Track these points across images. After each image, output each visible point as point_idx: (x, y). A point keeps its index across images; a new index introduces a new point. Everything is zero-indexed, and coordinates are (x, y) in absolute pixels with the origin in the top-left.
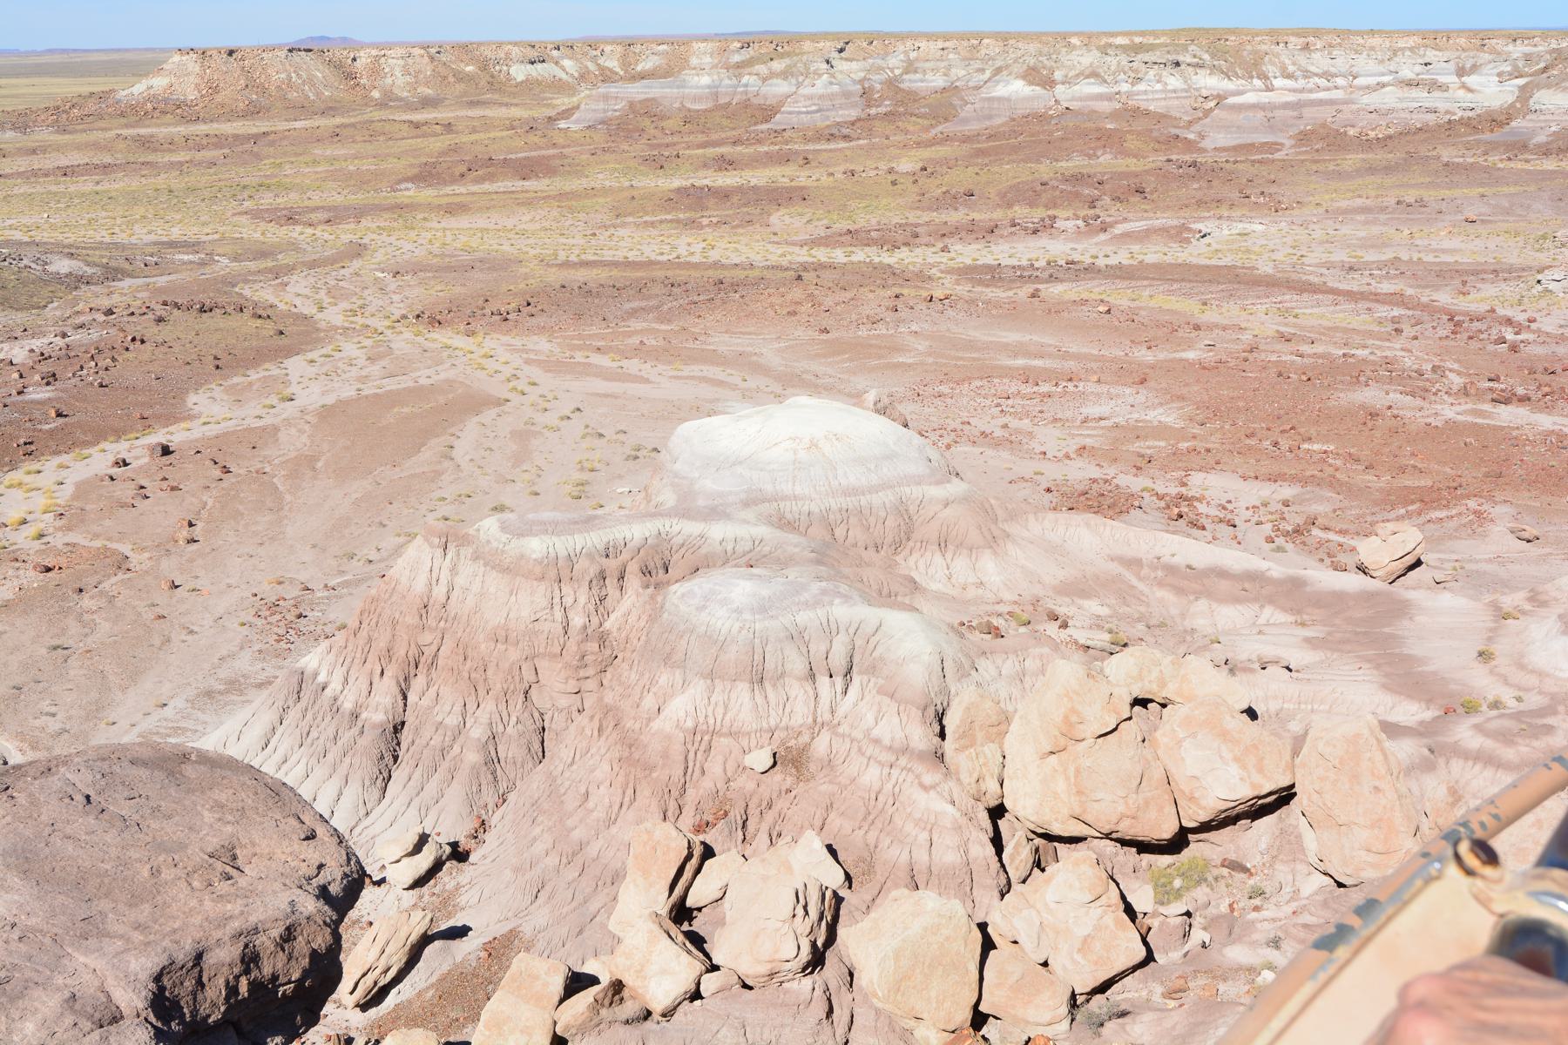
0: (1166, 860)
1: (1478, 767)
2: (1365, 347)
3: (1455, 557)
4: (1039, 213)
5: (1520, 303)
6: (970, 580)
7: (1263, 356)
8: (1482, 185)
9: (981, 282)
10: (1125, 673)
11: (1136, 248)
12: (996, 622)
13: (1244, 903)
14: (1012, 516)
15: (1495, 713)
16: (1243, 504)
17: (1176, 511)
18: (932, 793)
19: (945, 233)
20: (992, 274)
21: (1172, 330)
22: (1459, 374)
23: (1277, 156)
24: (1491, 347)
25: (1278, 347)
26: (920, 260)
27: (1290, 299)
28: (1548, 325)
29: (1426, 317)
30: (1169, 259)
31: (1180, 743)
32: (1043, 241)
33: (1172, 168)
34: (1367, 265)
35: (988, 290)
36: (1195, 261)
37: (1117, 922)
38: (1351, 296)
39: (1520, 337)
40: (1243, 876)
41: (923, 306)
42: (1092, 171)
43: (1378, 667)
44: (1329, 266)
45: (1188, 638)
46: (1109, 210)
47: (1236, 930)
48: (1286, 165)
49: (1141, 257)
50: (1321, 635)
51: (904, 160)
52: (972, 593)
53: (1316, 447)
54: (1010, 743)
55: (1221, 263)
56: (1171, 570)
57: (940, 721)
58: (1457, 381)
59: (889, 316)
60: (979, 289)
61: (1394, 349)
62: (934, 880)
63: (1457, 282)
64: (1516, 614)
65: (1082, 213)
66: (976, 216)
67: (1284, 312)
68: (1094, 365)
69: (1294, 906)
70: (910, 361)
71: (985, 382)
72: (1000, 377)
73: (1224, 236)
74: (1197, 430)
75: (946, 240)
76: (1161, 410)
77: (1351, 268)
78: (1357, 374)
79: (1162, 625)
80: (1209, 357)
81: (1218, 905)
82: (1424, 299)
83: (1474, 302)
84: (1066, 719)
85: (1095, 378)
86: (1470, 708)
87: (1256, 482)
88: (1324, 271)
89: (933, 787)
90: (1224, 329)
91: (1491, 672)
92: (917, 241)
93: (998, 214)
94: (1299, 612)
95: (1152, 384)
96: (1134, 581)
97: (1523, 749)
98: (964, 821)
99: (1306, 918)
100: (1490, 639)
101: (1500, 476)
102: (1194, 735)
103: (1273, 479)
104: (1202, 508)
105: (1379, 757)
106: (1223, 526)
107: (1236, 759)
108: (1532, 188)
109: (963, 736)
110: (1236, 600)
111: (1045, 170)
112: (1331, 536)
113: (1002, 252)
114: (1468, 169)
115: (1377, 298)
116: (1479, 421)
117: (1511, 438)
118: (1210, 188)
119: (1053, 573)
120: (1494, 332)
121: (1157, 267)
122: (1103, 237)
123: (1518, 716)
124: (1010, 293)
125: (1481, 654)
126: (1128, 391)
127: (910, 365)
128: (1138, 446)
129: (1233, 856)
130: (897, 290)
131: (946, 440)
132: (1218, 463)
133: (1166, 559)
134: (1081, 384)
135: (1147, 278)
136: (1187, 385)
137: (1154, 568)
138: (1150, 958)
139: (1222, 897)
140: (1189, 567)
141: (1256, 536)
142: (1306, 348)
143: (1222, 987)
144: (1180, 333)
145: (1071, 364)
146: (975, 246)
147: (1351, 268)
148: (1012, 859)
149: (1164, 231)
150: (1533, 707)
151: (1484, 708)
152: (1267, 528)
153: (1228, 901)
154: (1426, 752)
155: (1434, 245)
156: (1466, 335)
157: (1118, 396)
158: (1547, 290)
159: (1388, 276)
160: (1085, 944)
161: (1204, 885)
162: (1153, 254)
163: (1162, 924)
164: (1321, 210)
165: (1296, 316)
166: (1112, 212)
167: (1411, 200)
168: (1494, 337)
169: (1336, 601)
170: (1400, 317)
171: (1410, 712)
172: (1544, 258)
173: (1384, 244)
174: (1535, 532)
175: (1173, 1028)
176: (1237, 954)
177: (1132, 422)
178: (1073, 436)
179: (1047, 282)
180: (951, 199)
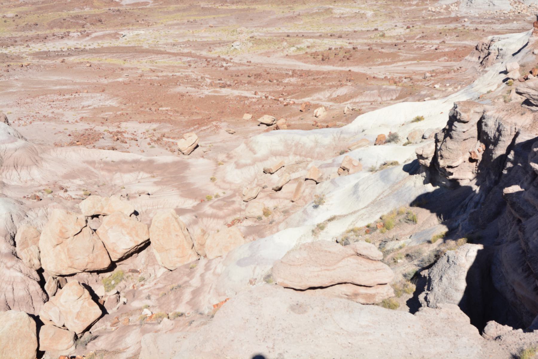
0: (108, 274)
1: (212, 219)
2: (179, 72)
3: (210, 142)
4: (64, 31)
5: (227, 53)
6: (28, 179)
7: (145, 78)
8: (214, 14)
9: (42, 58)
10: (87, 207)
11: (100, 42)
12: (37, 194)
13: (138, 284)
14: (44, 151)
15: (216, 199)
16: (140, 132)
17: (116, 137)
18: (12, 270)
19: (28, 40)
20: (47, 55)
21: (113, 71)
22: (209, 78)
23: (148, 6)
24: (219, 69)
25: (150, 74)
26: (18, 51)
27: (154, 57)
28: (236, 60)
29: (199, 60)
30: (112, 45)
31: (107, 231)
32: (65, 41)
33: (111, 12)
34: (179, 43)
35: (45, 61)
36: (121, 45)
37: (90, 304)
38: (175, 54)
39: (228, 65)
40: (137, 274)
41: (19, 69)
42: (82, 14)
43: (179, 189)
44: (167, 44)
45: (114, 188)
46: (89, 28)
47: (136, 294)
48: (151, 10)
49: (102, 45)
50: (160, 180)
51: (9, 12)
52: (29, 183)
53: (164, 109)
54: (41, 244)
55: (130, 45)
56: (106, 163)
57: (14, 239)
58: (209, 81)
59: (6, 74)
60: (42, 61)
61: (188, 72)
62: (16, 304)
63: (208, 47)
64: (223, 163)
65: (79, 30)
66: (39, 33)
67: (152, 61)
68: (86, 86)
69: (155, 281)
70: (15, 91)
71: (44, 96)
72: (50, 94)
73: (130, 36)
74: (123, 107)
75: (28, 43)
76: (110, 101)
77: (174, 45)
78: (176, 81)
79: (104, 185)
80: (127, 80)
81: (129, 287)
82: (198, 54)
83: (213, 54)
84: (61, 231)
85: (86, 91)
86: (209, 199)
87: (144, 124)
88: (165, 46)
89: (12, 267)
90: (132, 69)
91: (215, 185)
92: (16, 43)
93: (48, 32)
94: (152, 173)
95: (107, 91)
96: (93, 170)
97: (225, 211)
98: (26, 278)
99: (160, 286)
100: (215, 173)
101: (223, 112)
102: (112, 228)
103: (150, 122)
104: (125, 135)
105: (176, 224)
106: (133, 141)
107: (128, 233)
108: (229, 15)
109: (23, 243)
110: (130, 171)
111: (64, 14)
112: (170, 140)
113: (50, 46)
114: (211, 8)
115: (183, 54)
116: (216, 94)
117: (224, 99)
118: (125, 19)
119: (61, 171)
120: (220, 63)
121: (108, 48)
122: (88, 38)
123: (223, 199)
124: (54, 61)
125: (211, 179)
126: (98, 95)
127: (14, 92)
128: (102, 115)
129: (132, 268)
130: (9, 63)
131: (30, 120)
132: (131, 118)
133: (104, 159)
134: (81, 94)
135: (104, 53)
136: (119, 91)
137: (100, 163)
138: (104, 312)
139: (130, 283)
140: (113, 161)
141: (144, 144)
142: (160, 74)
143: (131, 318)
144: (117, 72)
145: (77, 87)
146: (39, 44)
147: (174, 45)
148: (48, 287)
149: (110, 35)
150: (229, 195)
151: (213, 198)
152: (148, 140)
153: (132, 285)
154: (194, 217)
155: (200, 35)
156: (211, 66)
157: (94, 97)
158: (235, 49)
159: (186, 47)
160: (78, 315)
161: (123, 281)
162: (106, 43)
163: (109, 299)
164: (163, 25)
165: (156, 63)
166: (91, 29)
167: (191, 20)
168: (220, 65)
169: (164, 167)
170: (190, 61)
171: (189, 204)
172: (234, 38)
173: (183, 36)
174: (234, 130)
175: (112, 340)
176: (136, 304)
177: (100, 106)
178: (79, 114)
179: (67, 56)
180: (28, 27)
